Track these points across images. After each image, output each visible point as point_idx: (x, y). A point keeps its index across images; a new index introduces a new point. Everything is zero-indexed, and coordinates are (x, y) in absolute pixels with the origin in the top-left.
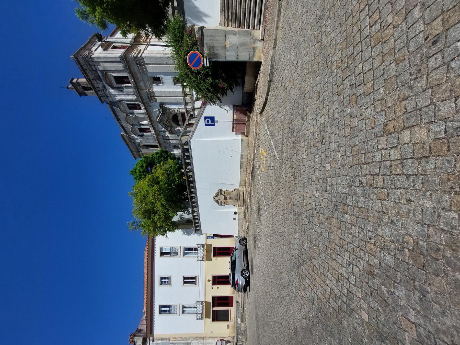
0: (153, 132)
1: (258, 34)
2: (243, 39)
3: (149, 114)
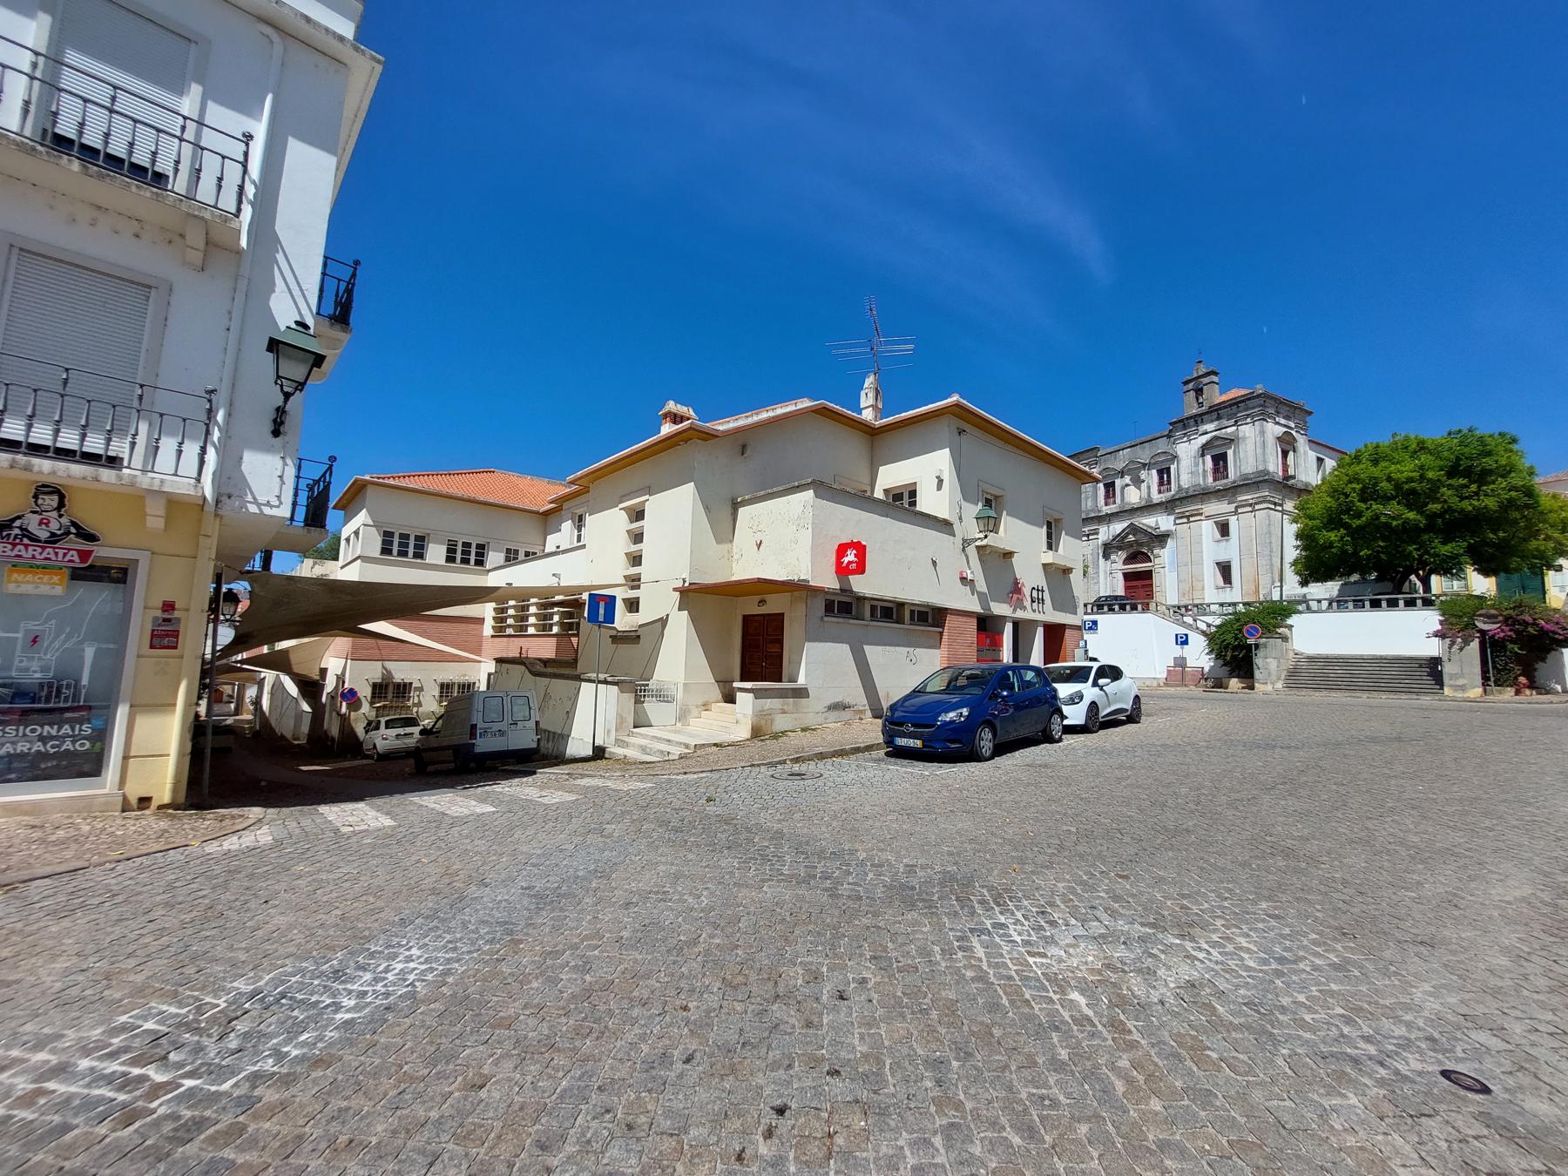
0: (1106, 510)
1: (1279, 685)
2: (1274, 673)
3: (1149, 508)
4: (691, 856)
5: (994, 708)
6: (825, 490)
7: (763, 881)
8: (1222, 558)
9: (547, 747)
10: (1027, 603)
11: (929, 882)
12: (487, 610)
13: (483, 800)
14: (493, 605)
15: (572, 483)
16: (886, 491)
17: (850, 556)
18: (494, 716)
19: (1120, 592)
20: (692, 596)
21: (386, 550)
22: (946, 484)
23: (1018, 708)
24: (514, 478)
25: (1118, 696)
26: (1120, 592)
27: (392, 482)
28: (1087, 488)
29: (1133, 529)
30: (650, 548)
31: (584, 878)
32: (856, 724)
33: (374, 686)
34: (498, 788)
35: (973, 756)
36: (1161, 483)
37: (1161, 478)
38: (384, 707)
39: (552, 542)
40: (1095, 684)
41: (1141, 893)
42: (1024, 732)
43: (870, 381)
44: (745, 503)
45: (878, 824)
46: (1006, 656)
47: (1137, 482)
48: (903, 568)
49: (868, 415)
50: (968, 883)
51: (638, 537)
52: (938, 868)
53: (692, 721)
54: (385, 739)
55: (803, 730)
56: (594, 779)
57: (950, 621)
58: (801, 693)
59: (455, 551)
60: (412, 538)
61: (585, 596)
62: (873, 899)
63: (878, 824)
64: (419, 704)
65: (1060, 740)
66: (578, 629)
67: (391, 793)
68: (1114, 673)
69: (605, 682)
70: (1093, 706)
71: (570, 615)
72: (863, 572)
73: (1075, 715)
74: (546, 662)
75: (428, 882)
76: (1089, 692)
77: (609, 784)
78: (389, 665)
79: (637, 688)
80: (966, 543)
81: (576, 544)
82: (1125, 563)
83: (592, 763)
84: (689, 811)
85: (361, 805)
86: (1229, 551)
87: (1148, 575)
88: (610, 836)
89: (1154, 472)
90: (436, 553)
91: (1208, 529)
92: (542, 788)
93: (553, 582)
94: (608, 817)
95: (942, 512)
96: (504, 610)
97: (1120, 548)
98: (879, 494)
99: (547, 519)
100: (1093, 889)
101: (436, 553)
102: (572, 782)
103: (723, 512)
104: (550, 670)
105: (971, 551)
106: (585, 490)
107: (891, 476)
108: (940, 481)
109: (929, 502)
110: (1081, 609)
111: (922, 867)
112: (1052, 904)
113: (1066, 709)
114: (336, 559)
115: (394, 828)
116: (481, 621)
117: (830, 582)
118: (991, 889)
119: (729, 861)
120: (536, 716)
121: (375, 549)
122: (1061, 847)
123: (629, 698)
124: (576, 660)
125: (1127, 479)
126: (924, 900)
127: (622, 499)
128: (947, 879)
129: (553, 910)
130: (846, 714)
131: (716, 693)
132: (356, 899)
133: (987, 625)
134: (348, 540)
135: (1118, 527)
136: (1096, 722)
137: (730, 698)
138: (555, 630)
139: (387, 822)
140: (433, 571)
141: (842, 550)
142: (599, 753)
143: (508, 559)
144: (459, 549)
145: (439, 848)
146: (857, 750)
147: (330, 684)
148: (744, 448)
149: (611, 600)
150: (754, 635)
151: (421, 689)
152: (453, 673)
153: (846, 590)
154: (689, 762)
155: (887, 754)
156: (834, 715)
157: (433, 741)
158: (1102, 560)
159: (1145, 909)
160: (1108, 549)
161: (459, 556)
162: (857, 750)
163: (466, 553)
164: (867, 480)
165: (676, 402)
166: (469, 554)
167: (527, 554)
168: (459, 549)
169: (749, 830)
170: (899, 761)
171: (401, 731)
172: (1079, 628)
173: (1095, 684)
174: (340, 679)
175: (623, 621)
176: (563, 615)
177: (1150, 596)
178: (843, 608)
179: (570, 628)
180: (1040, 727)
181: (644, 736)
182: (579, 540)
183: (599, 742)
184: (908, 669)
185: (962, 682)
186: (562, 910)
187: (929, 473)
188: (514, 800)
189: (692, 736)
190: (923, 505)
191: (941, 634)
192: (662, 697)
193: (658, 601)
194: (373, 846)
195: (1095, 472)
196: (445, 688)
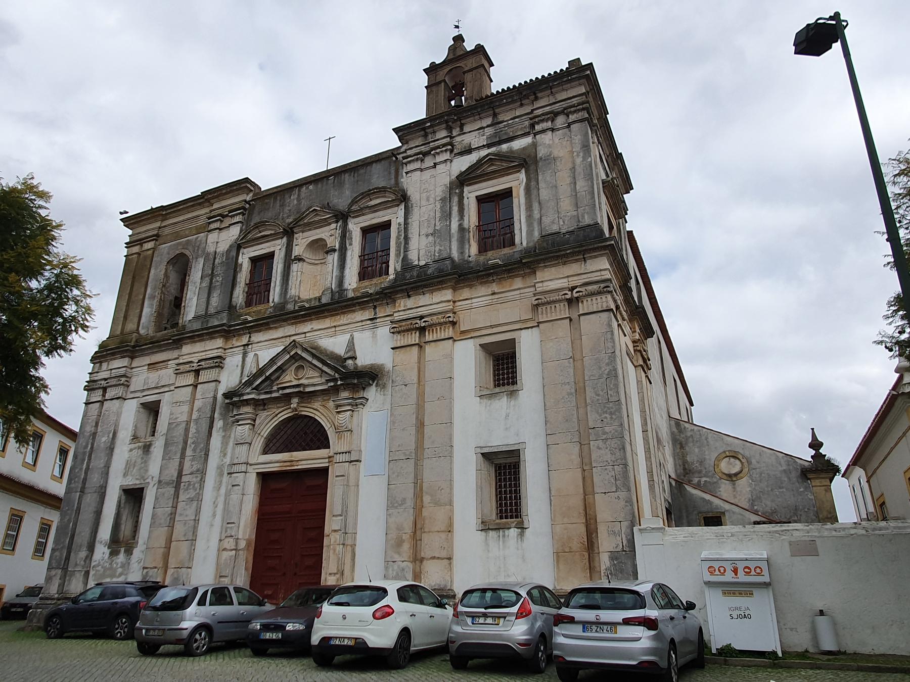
8: (499, 441)
29: (295, 356)
82: (272, 445)
86: (521, 421)
91: (465, 361)
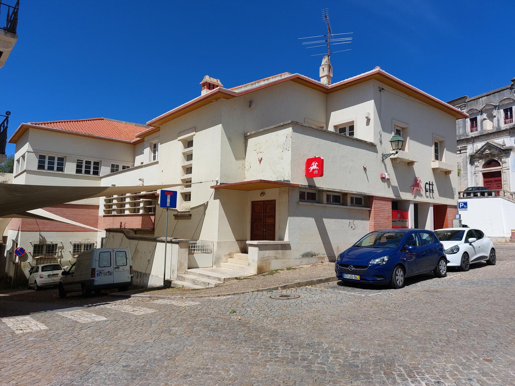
3: (499, 133)
4: (223, 346)
5: (403, 256)
6: (299, 127)
7: (266, 361)
9: (137, 281)
10: (423, 192)
11: (367, 362)
12: (101, 201)
13: (99, 313)
14: (104, 198)
15: (150, 125)
16: (335, 127)
17: (314, 166)
18: (105, 263)
19: (481, 184)
20: (222, 190)
21: (41, 166)
22: (372, 122)
23: (418, 256)
24: (115, 123)
25: (481, 249)
26: (481, 184)
27: (43, 126)
28: (460, 121)
30: (196, 162)
31: (160, 360)
32: (319, 265)
33: (35, 246)
34: (108, 306)
35: (391, 285)
36: (506, 117)
37: (506, 114)
38: (41, 258)
39: (139, 160)
40: (466, 241)
41: (500, 371)
42: (423, 271)
43: (325, 61)
44: (252, 136)
45: (334, 327)
46: (410, 224)
47: (491, 117)
48: (348, 172)
49: (324, 81)
50: (391, 364)
51: (189, 157)
52: (372, 354)
53: (222, 264)
54: (42, 277)
55: (288, 269)
56: (164, 300)
57: (376, 204)
58: (286, 247)
59: (81, 166)
60: (56, 159)
61: (159, 192)
62: (332, 373)
63: (334, 327)
64: (62, 257)
65: (445, 276)
66: (155, 211)
67: (45, 310)
68: (478, 234)
69: (171, 242)
70: (466, 255)
71: (150, 203)
72: (322, 175)
73: (454, 260)
74: (136, 231)
75: (67, 364)
76: (463, 246)
77: (174, 302)
78: (44, 234)
79: (190, 247)
80: (385, 156)
81: (152, 161)
83: (163, 291)
84: (222, 319)
85: (27, 317)
87: (498, 174)
88: (175, 334)
89: (502, 111)
90: (70, 168)
92: (134, 306)
93: (140, 184)
94: (173, 323)
95: (370, 138)
96: (110, 201)
97: (481, 158)
98: (331, 129)
99: (136, 147)
100: (469, 368)
101: (70, 168)
102: (151, 301)
103: (239, 141)
104: (138, 236)
105: (388, 161)
106: (157, 130)
107: (338, 117)
108: (368, 120)
109: (363, 132)
110: (456, 196)
111: (363, 354)
112: (444, 377)
113: (448, 257)
114: (11, 172)
115: (46, 331)
116: (97, 207)
117: (303, 182)
118: (405, 367)
119: (246, 349)
120: (130, 263)
121: (34, 166)
122: (448, 342)
123: (185, 251)
124: (153, 230)
125: (485, 116)
126: (364, 374)
127: (180, 134)
128: (378, 361)
129: (141, 380)
130: (313, 260)
131: (236, 247)
132: (25, 374)
133: (398, 207)
134: (18, 161)
135: (479, 145)
136: (467, 264)
137: (244, 251)
138: (141, 212)
139: (43, 327)
140: (68, 179)
141: (309, 162)
142: (168, 284)
143: (112, 171)
144: (84, 165)
145: (74, 343)
146: (320, 281)
147: (9, 245)
148: (250, 103)
149: (174, 194)
150: (259, 214)
151: (62, 248)
152: (81, 238)
153: (312, 186)
154: (221, 289)
155: (339, 284)
156: (306, 260)
157: (70, 279)
158: (469, 166)
159: (503, 381)
160: (473, 159)
161: (84, 169)
162: (320, 281)
163: (88, 167)
164: (323, 120)
165: (210, 76)
166: (90, 168)
167: (124, 168)
168: (84, 165)
169: (257, 330)
170: (346, 288)
171: (51, 273)
172: (455, 207)
173: (466, 241)
174: (15, 243)
175: (181, 206)
176: (146, 203)
177: (500, 187)
178: (311, 198)
179: (150, 211)
180: (433, 268)
181: (194, 274)
182: (154, 159)
183: (167, 278)
184: (350, 233)
185: (384, 240)
186: (147, 379)
187: (362, 115)
188: (117, 313)
189: (222, 273)
190: (358, 135)
191: (370, 211)
192: (205, 250)
193: (202, 194)
194: (34, 342)
195: (465, 111)
196: (77, 247)
